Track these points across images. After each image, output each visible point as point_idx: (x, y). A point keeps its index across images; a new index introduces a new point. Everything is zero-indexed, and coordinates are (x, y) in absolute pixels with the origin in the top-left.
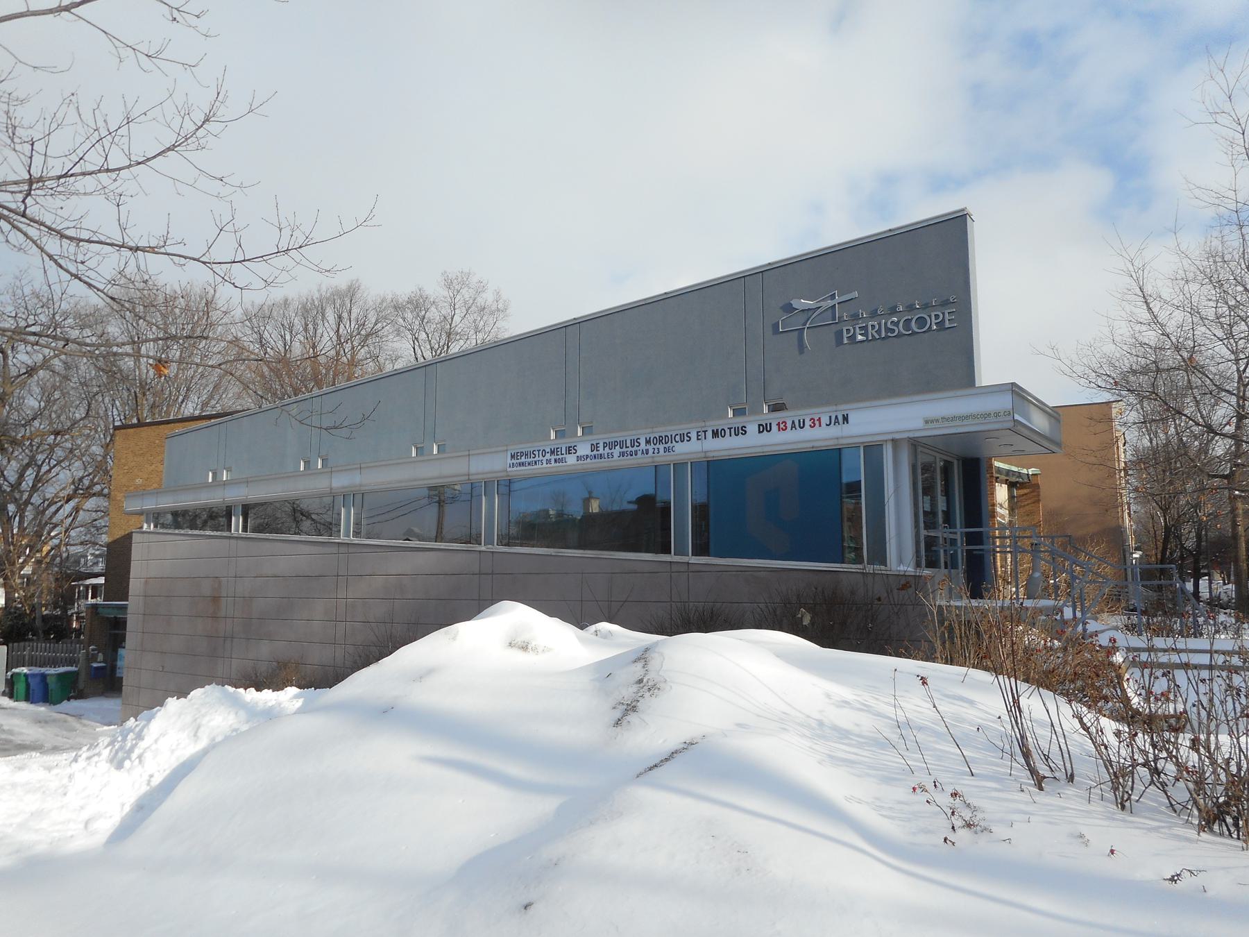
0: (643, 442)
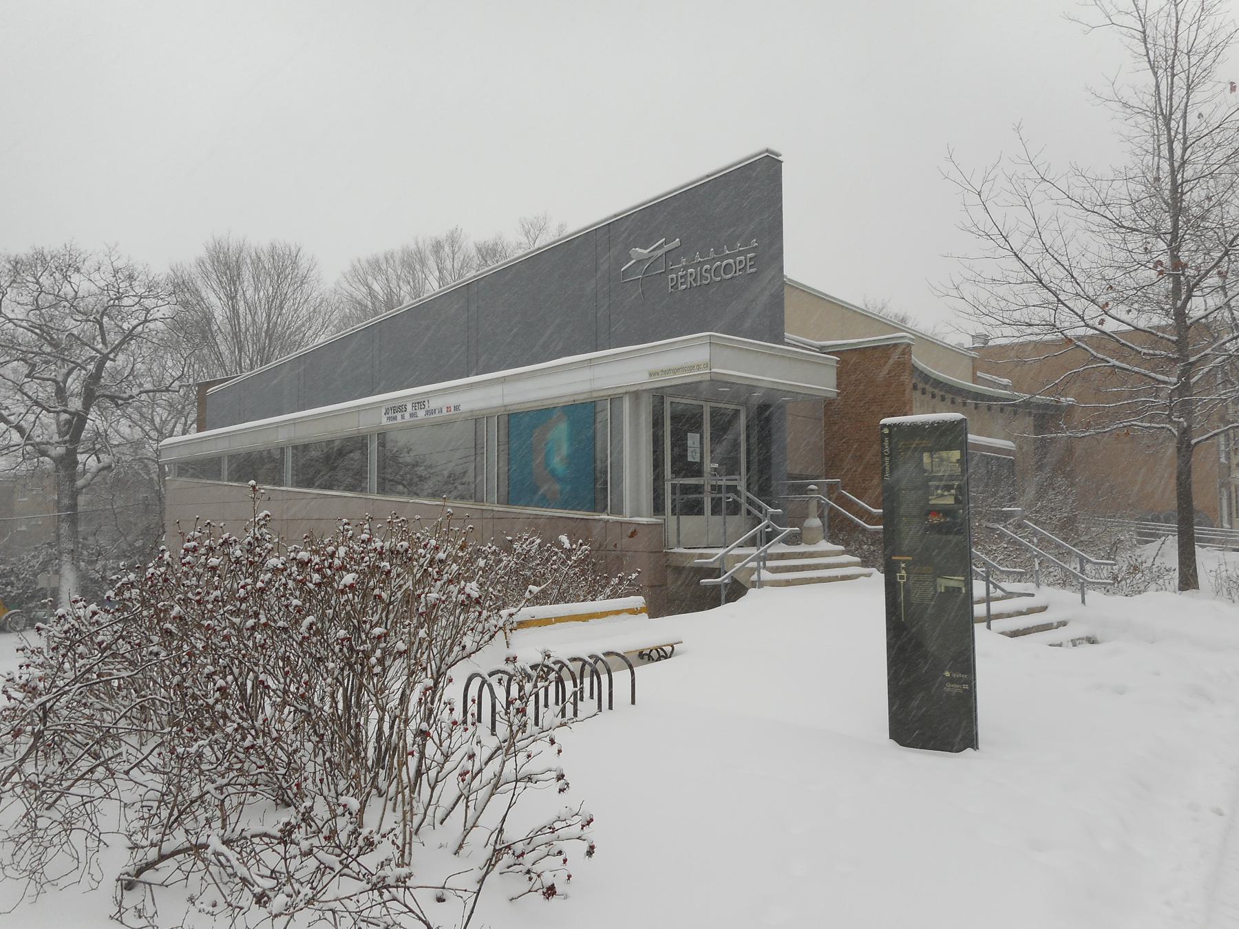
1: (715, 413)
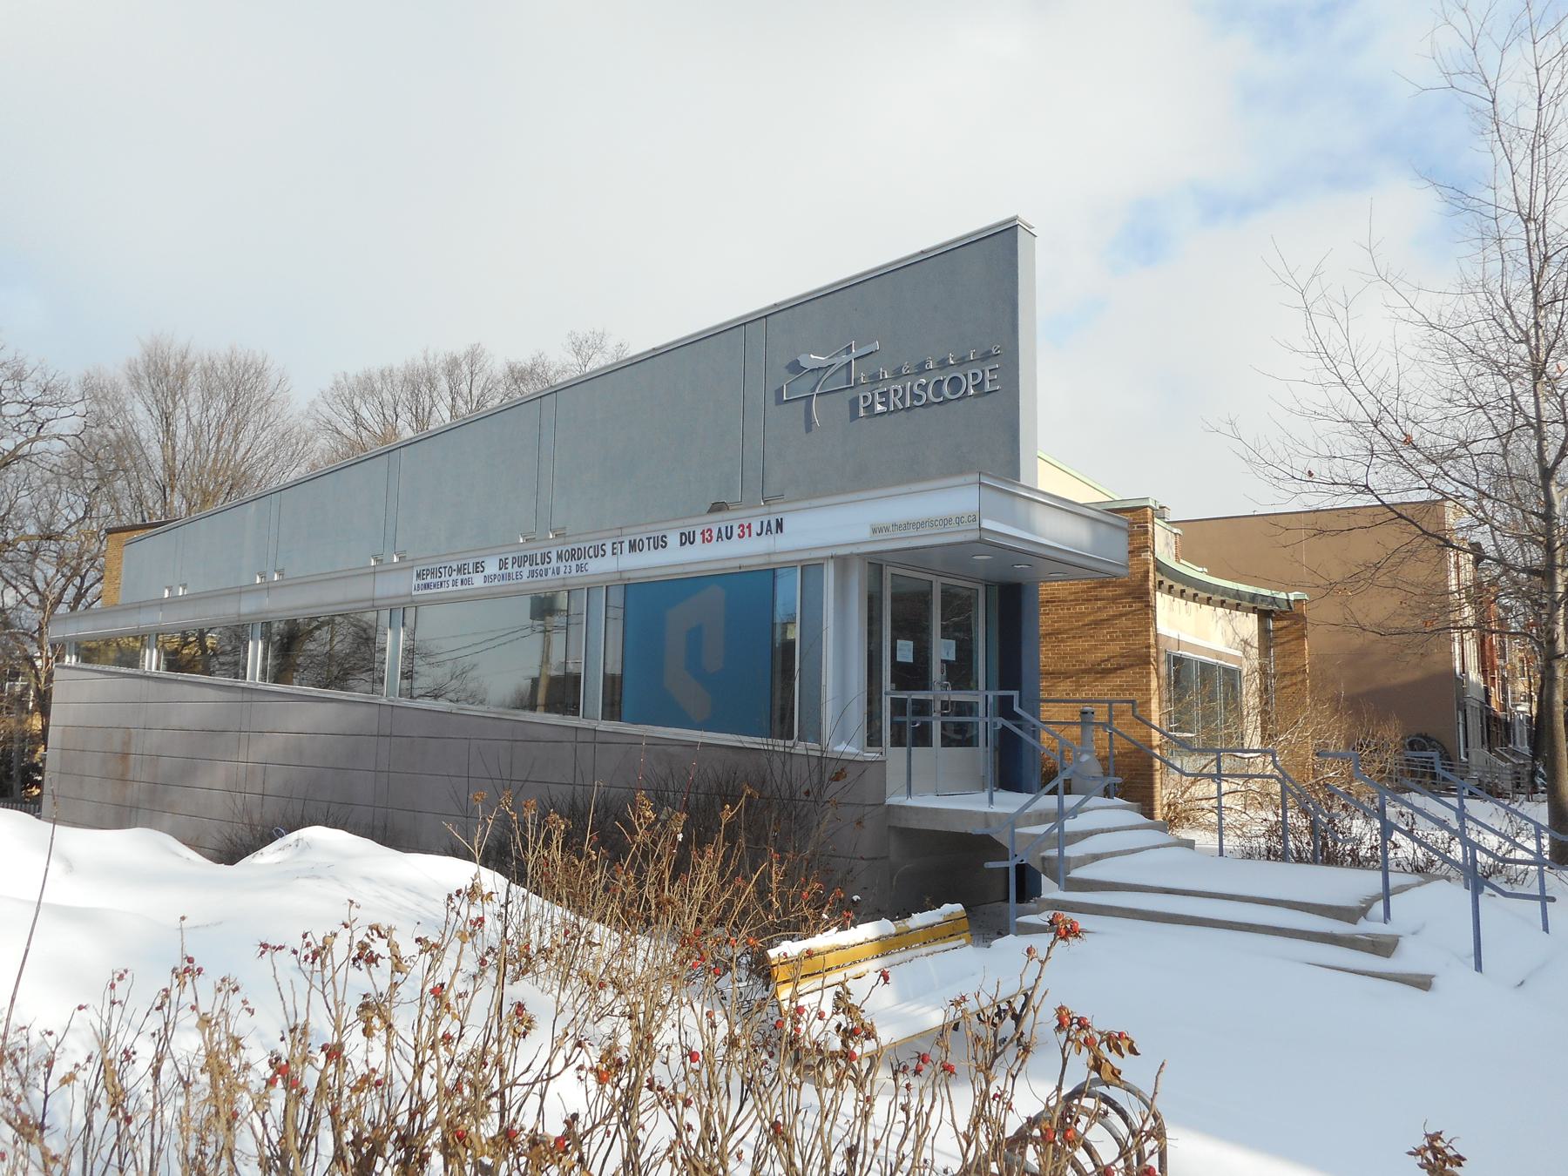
0: (554, 556)
1: (948, 595)
